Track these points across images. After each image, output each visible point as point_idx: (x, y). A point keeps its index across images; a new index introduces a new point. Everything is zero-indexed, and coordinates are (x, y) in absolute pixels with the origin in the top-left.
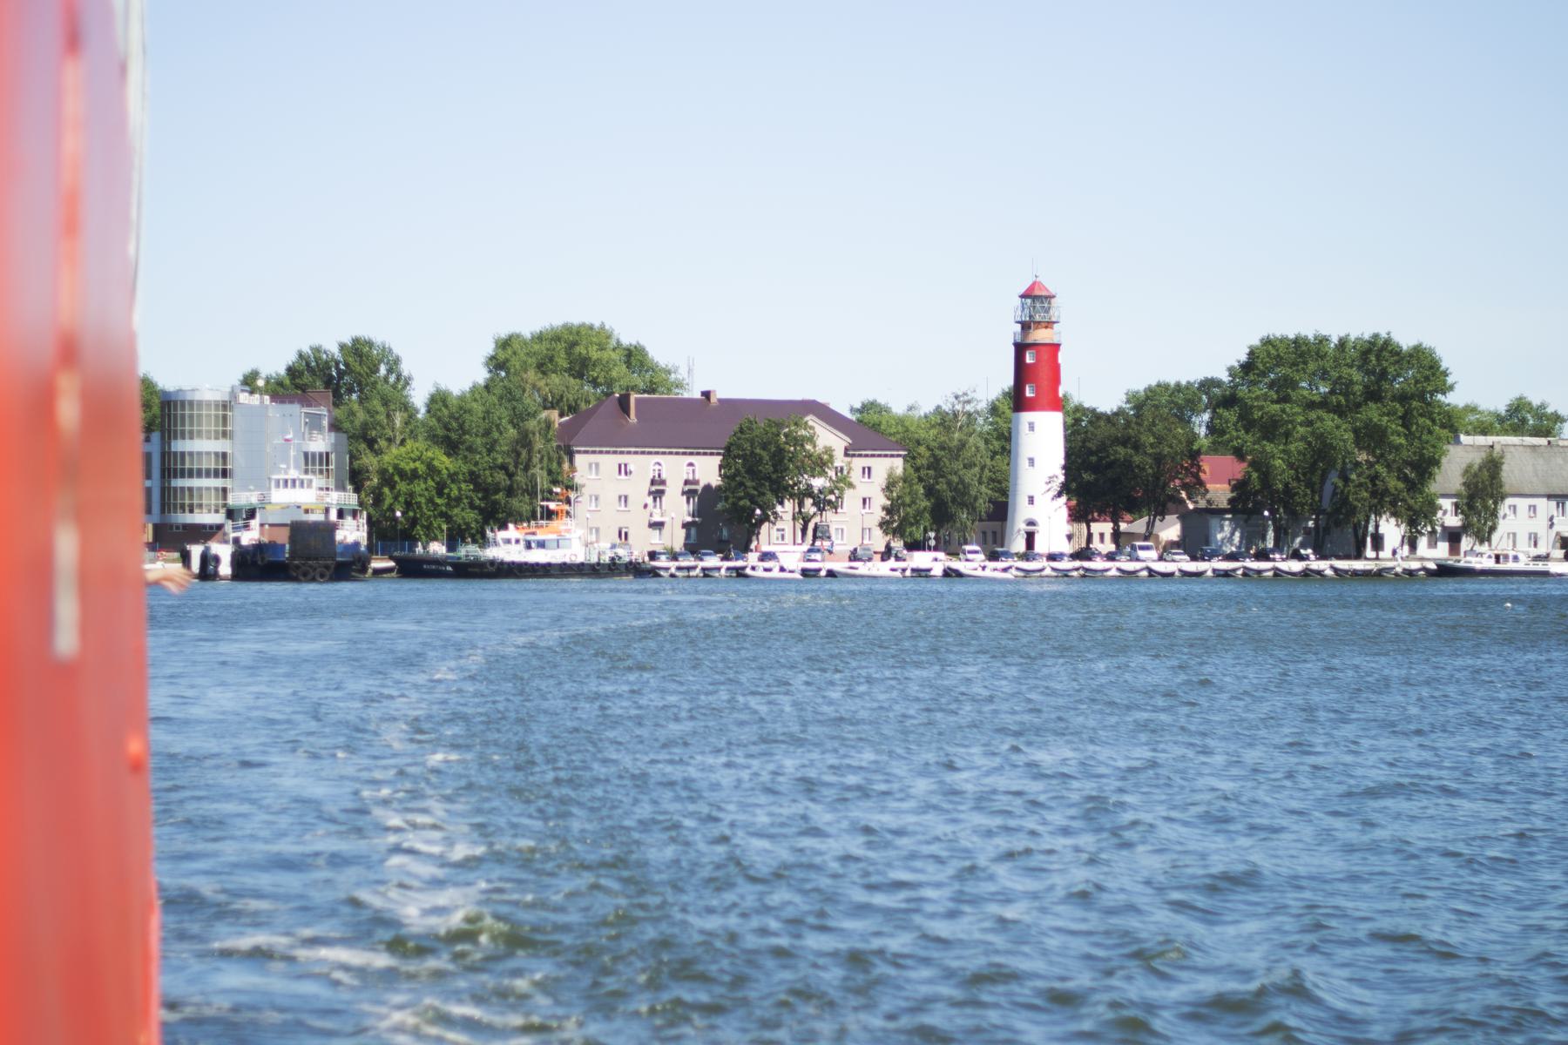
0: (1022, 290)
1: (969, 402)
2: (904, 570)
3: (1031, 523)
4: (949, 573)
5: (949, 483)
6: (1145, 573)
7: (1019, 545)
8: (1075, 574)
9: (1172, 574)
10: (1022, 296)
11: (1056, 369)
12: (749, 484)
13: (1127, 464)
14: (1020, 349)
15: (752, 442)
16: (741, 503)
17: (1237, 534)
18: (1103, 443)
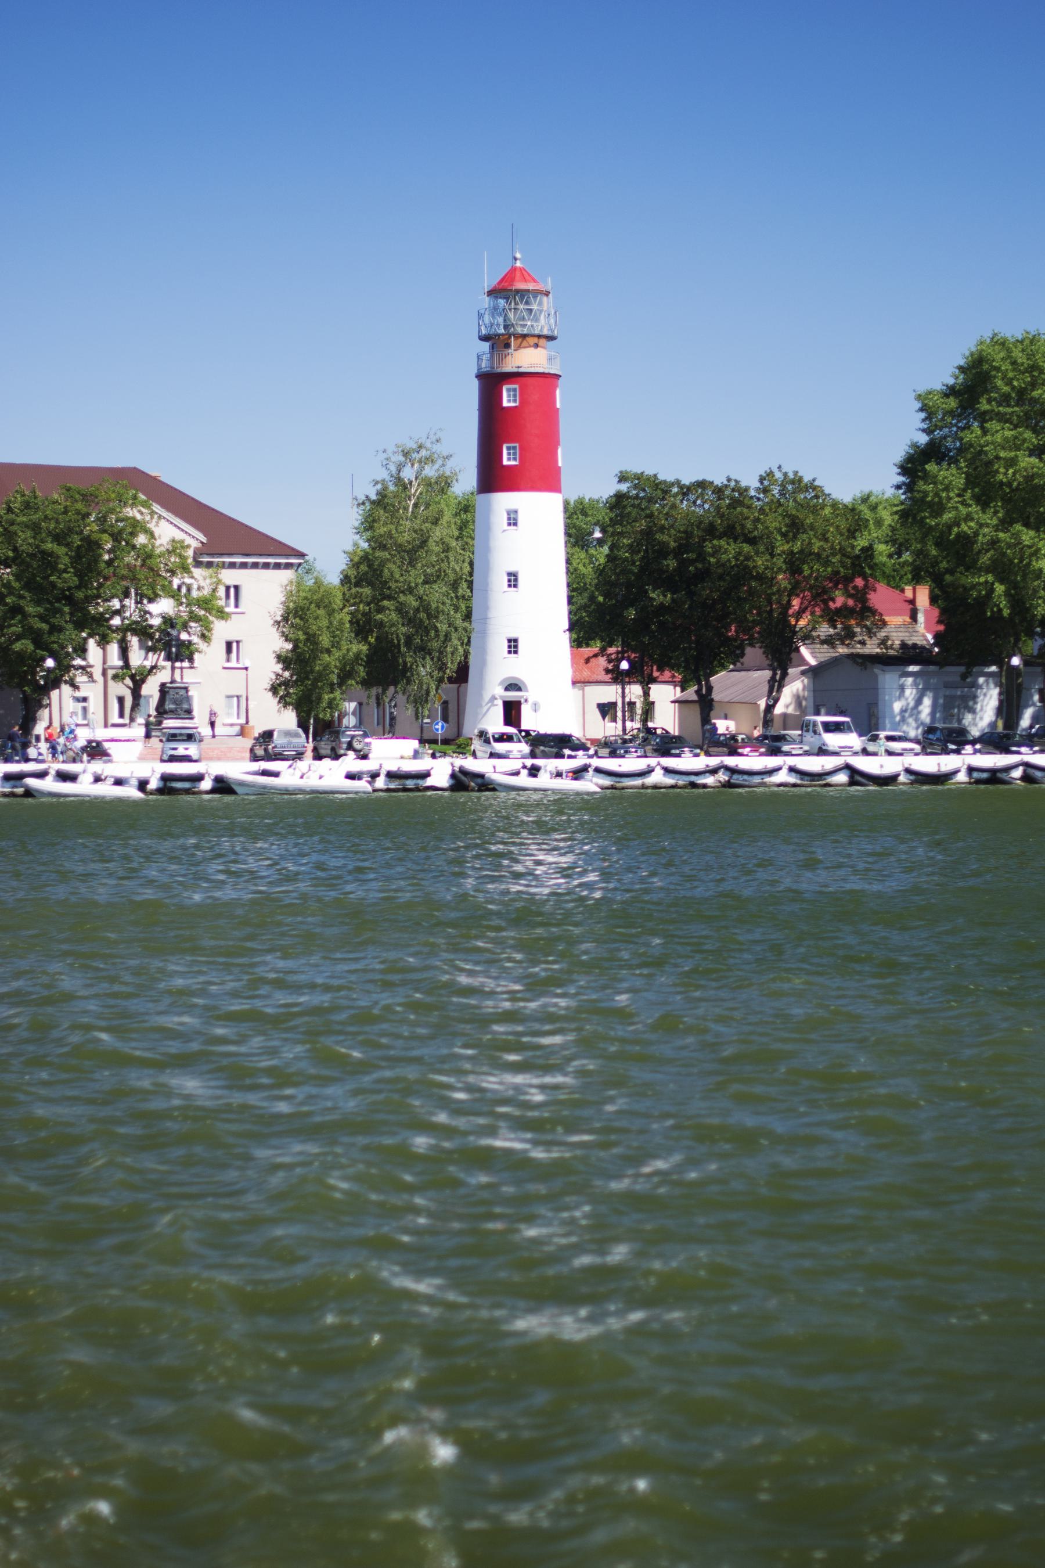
0: (490, 281)
1: (430, 460)
2: (374, 776)
3: (513, 686)
4: (461, 781)
5: (400, 609)
6: (842, 778)
7: (494, 723)
8: (710, 780)
9: (892, 779)
10: (490, 293)
11: (551, 415)
12: (30, 609)
13: (743, 573)
14: (491, 383)
15: (35, 528)
16: (17, 646)
17: (927, 702)
18: (688, 534)
